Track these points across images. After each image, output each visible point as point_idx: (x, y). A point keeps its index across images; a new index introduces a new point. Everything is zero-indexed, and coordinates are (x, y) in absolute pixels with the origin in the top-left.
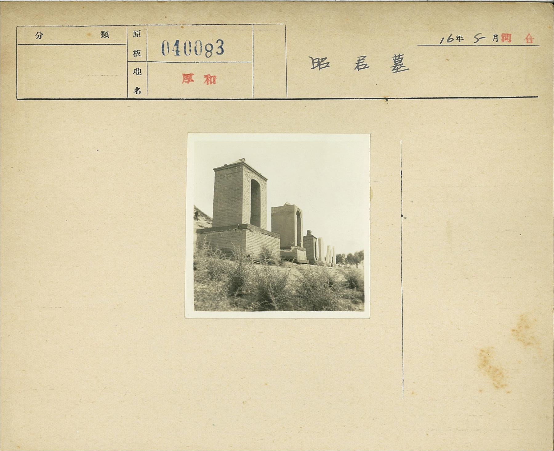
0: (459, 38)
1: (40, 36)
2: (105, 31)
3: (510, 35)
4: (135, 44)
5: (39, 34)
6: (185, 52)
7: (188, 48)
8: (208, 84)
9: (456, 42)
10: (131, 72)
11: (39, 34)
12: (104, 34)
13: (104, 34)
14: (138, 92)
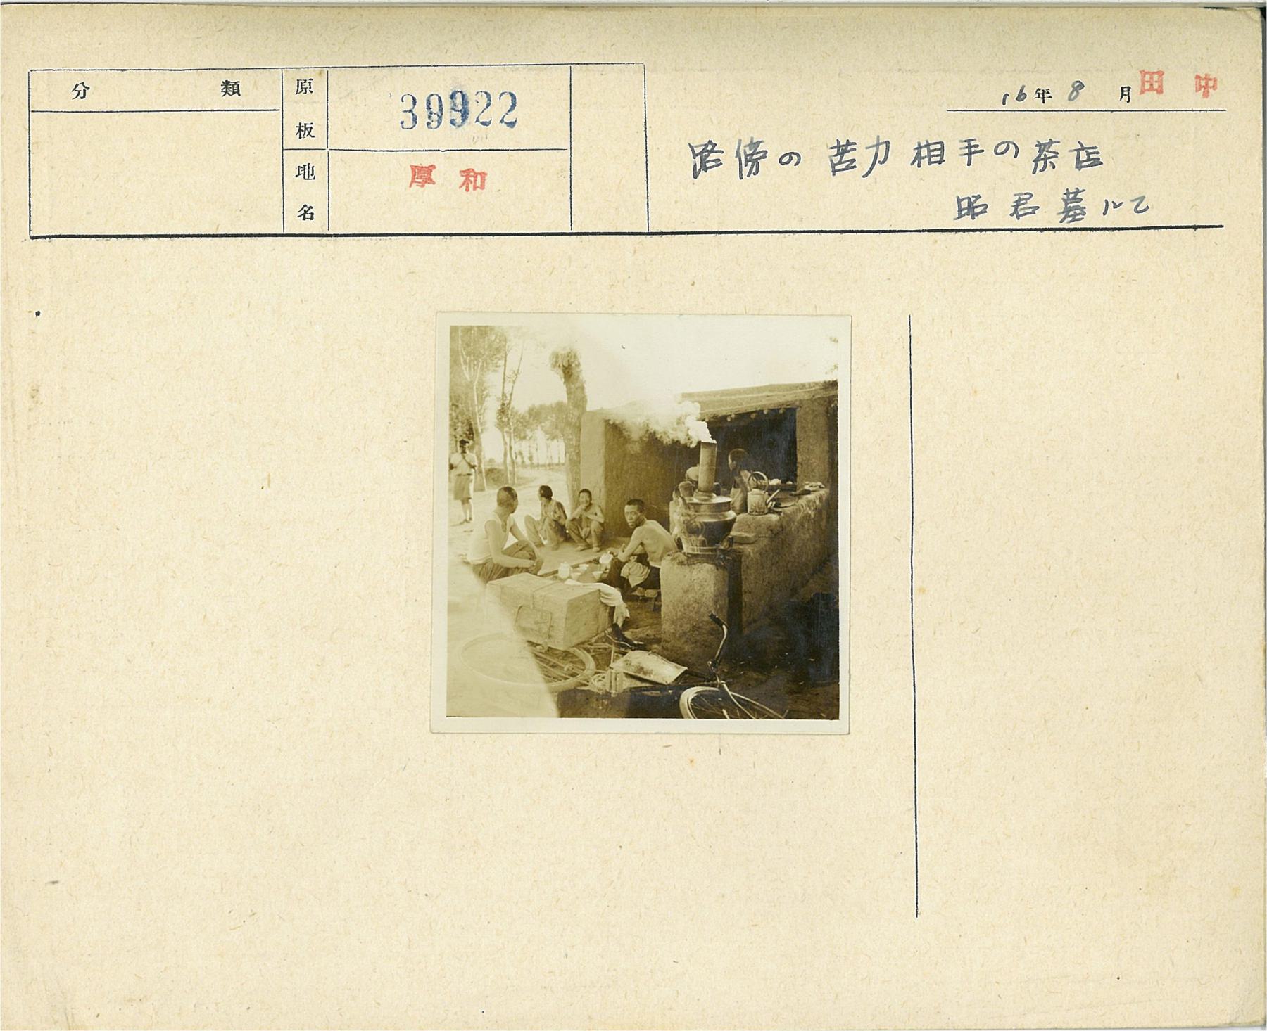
0: (1042, 95)
1: (82, 91)
2: (232, 80)
3: (1161, 74)
4: (306, 109)
5: (81, 88)
6: (440, 100)
7: (435, 108)
8: (467, 190)
9: (1031, 101)
10: (291, 170)
11: (81, 88)
12: (230, 88)
13: (230, 88)
14: (308, 216)
